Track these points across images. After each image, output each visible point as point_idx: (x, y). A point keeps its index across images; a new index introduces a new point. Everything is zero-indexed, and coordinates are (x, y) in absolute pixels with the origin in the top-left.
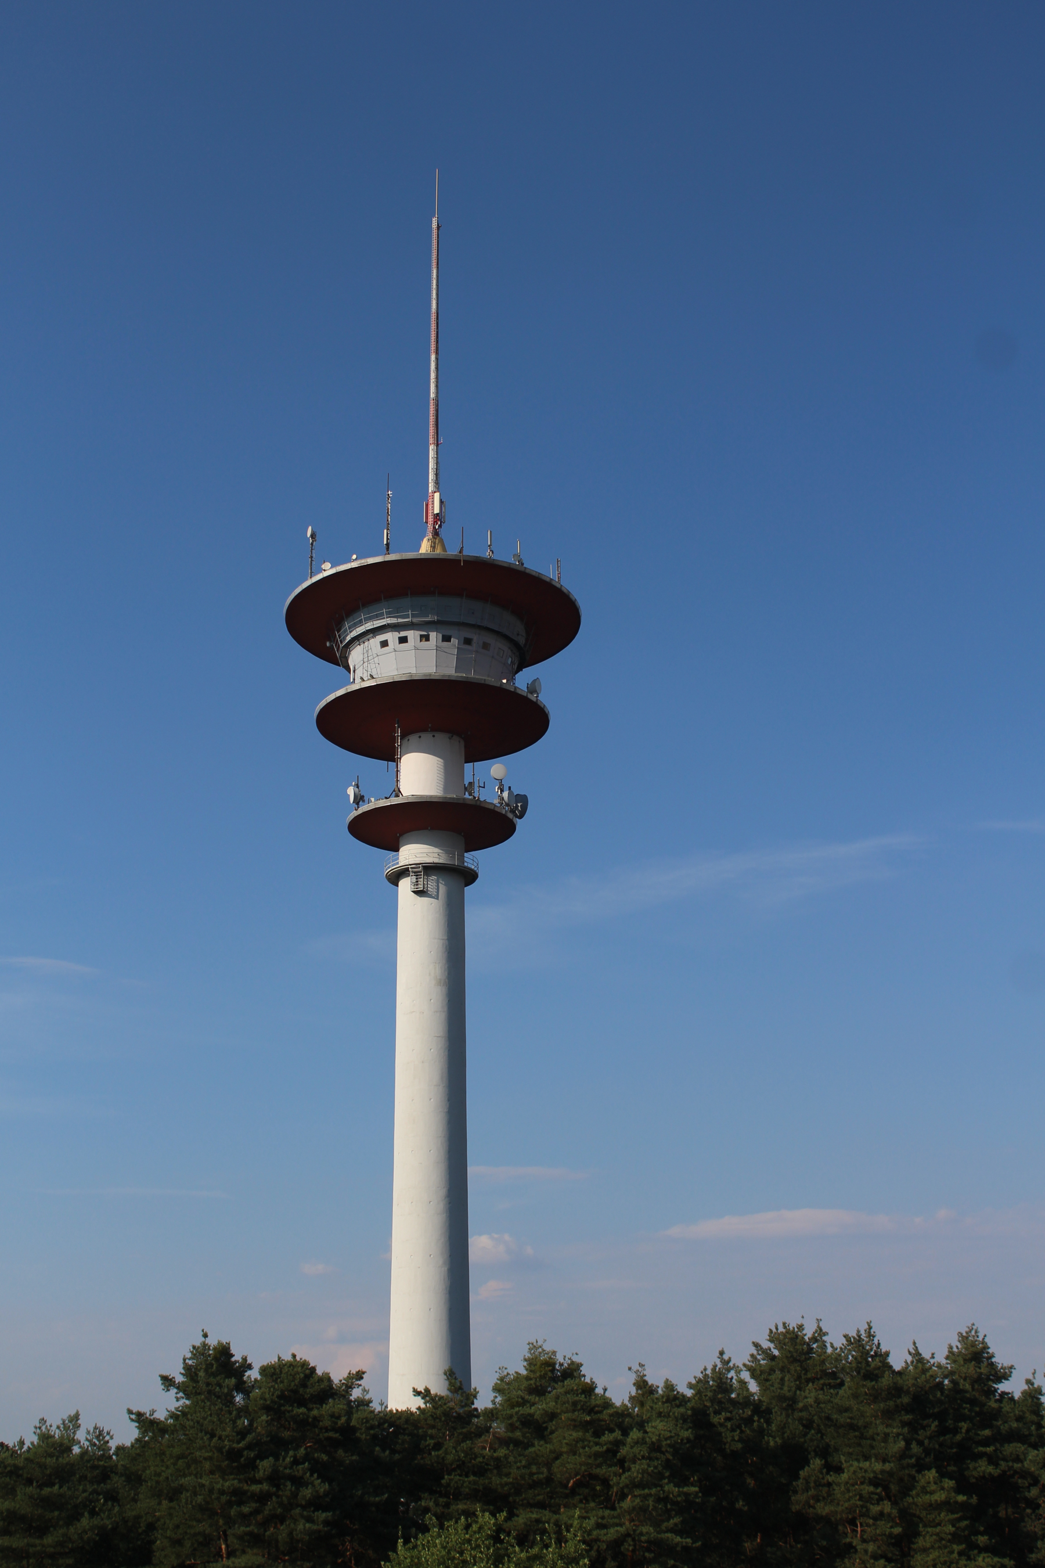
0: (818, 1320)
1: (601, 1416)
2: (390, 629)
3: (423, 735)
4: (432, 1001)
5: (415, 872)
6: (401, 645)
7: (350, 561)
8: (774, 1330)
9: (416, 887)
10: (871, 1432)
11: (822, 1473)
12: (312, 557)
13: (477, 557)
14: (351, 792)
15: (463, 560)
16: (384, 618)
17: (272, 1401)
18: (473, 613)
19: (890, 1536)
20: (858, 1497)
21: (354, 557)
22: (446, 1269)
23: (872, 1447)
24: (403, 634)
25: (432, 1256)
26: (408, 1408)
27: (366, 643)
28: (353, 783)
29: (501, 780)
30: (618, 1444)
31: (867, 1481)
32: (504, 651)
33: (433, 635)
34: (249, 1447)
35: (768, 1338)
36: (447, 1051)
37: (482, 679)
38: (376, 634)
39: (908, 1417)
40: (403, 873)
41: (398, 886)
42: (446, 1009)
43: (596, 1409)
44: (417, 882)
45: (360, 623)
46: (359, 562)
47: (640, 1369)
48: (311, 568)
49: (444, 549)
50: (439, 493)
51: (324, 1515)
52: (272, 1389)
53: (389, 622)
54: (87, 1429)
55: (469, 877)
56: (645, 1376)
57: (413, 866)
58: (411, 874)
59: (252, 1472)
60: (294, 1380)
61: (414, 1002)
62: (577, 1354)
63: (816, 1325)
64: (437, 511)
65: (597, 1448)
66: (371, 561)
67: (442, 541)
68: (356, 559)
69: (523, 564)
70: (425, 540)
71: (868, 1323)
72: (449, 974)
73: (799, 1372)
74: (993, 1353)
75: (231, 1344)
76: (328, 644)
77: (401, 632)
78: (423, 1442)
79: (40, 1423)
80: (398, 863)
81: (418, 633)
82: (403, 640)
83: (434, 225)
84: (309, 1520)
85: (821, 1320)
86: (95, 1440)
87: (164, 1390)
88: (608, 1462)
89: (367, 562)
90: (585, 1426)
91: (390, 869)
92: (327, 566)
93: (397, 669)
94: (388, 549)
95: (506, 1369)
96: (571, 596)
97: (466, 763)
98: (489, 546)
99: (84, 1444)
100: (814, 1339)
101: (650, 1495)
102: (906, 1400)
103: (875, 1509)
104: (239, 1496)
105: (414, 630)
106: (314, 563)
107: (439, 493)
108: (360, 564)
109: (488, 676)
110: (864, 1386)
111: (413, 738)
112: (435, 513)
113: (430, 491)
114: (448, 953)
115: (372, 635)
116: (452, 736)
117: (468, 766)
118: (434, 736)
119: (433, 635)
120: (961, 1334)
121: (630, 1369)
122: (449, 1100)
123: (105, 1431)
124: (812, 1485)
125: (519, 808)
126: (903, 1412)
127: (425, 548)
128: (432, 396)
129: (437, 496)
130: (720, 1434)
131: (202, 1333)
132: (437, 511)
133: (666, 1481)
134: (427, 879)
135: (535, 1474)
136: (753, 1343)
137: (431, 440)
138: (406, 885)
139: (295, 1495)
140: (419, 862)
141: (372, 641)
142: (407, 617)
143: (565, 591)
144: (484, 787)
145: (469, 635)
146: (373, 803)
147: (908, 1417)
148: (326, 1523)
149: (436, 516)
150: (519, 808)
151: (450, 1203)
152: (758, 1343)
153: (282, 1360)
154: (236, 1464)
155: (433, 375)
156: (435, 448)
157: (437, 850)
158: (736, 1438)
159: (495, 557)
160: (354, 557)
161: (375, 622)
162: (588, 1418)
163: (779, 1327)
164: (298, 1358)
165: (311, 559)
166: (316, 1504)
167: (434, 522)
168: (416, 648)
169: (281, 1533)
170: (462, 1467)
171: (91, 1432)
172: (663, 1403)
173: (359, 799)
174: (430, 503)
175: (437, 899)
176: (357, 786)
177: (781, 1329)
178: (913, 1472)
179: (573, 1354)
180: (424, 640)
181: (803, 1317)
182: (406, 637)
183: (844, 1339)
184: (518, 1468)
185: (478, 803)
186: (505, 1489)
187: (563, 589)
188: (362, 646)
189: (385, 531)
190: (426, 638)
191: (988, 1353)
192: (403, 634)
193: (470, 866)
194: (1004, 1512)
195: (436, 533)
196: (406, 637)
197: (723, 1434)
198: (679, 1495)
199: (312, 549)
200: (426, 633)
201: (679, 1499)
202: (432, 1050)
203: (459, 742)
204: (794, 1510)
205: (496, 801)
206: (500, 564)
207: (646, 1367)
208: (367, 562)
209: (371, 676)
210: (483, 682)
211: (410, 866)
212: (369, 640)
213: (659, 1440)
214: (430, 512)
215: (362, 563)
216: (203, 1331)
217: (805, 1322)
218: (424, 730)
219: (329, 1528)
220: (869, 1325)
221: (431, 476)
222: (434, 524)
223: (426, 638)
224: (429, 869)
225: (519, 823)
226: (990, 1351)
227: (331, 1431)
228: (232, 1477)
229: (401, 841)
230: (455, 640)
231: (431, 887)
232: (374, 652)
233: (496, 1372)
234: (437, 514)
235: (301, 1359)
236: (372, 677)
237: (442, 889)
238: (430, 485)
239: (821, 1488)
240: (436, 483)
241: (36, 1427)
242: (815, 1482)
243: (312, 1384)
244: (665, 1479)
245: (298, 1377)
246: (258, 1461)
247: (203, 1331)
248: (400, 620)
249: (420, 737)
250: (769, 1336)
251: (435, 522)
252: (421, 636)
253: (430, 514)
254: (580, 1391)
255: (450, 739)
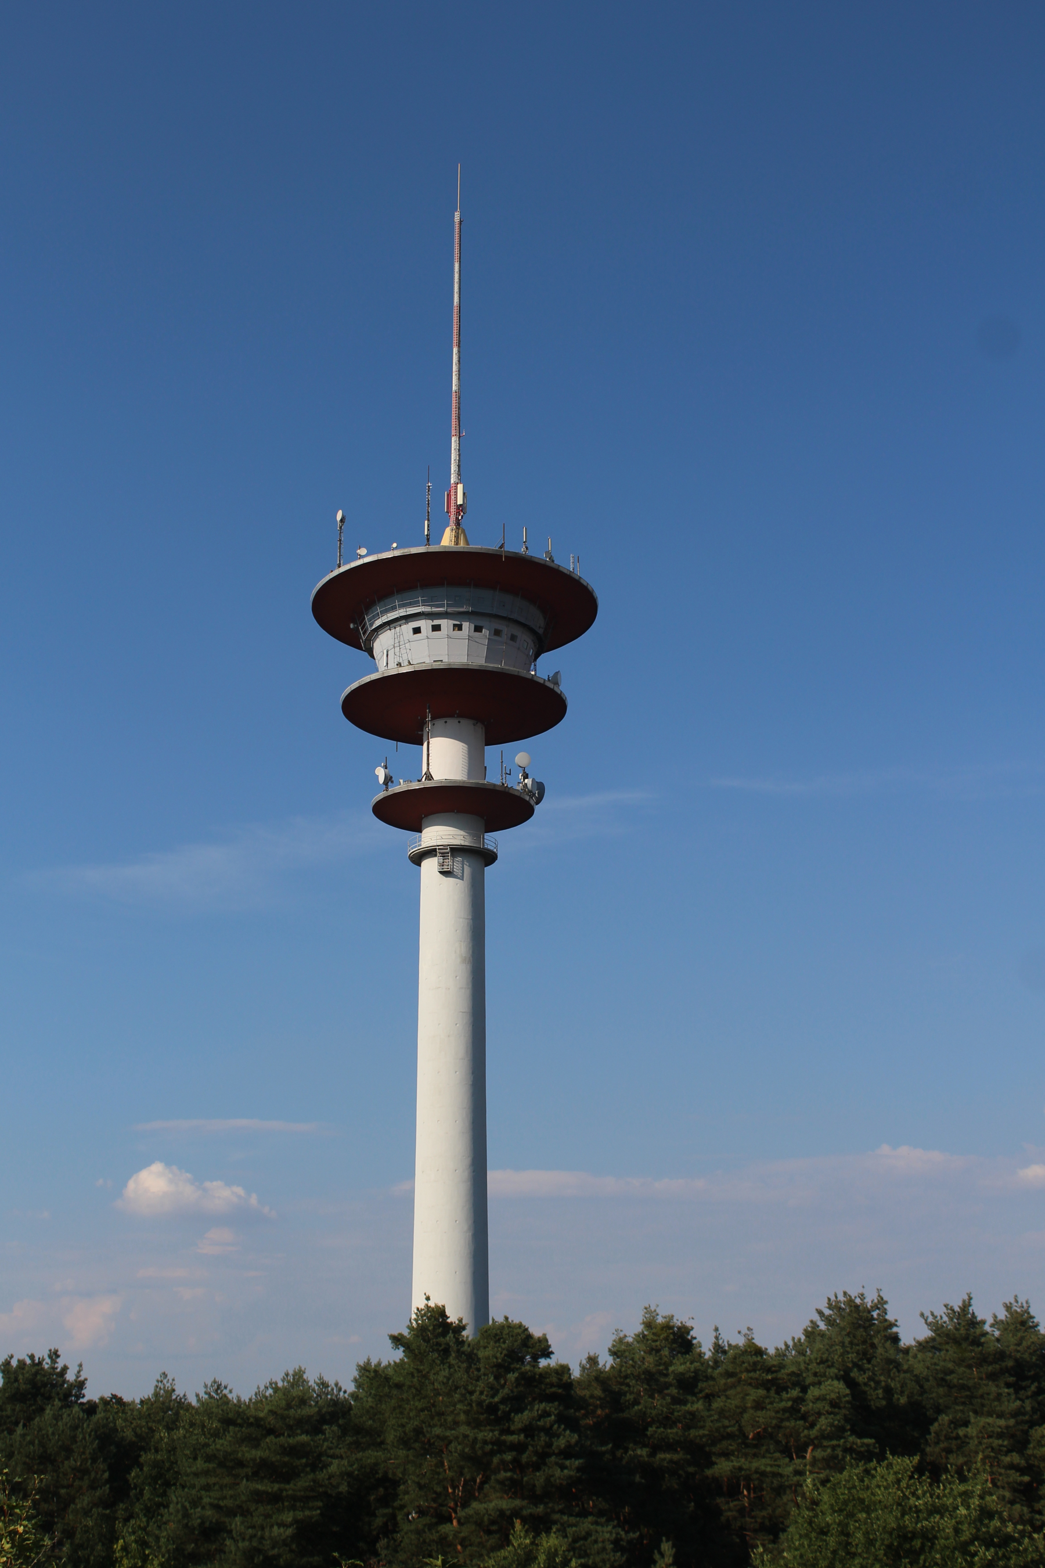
0: (878, 1290)
1: (779, 1375)
2: (424, 617)
3: (449, 720)
4: (458, 978)
5: (442, 853)
6: (434, 632)
7: (389, 549)
8: (833, 1298)
9: (441, 867)
10: (980, 1392)
11: (950, 1428)
12: (340, 540)
13: (516, 553)
14: (381, 773)
15: (505, 556)
16: (419, 606)
17: (503, 1360)
18: (504, 606)
19: (1021, 1483)
20: (990, 1450)
21: (395, 545)
22: (470, 1234)
23: (983, 1405)
24: (436, 622)
25: (457, 1222)
26: (300, 1367)
27: (398, 629)
28: (382, 764)
29: (524, 768)
30: (799, 1400)
31: (995, 1435)
32: (528, 643)
33: (466, 625)
34: (503, 1401)
35: (827, 1305)
36: (471, 1026)
37: (515, 671)
38: (409, 620)
39: (1012, 1379)
40: (430, 852)
41: (420, 866)
42: (470, 986)
43: (773, 1369)
44: (443, 862)
45: (394, 609)
46: (402, 552)
47: (748, 1333)
48: (340, 551)
49: (467, 542)
50: (462, 485)
51: (577, 1462)
52: (500, 1349)
53: (423, 610)
54: (205, 1383)
55: (489, 858)
56: (753, 1339)
57: (441, 847)
58: (438, 855)
59: (507, 1424)
60: (516, 1341)
61: (440, 978)
62: (693, 1318)
63: (877, 1294)
64: (460, 502)
65: (783, 1404)
66: (414, 550)
67: (464, 531)
68: (396, 548)
69: (553, 561)
70: (448, 531)
71: (967, 1294)
72: (473, 952)
73: (865, 1337)
74: (1038, 1322)
75: (446, 1307)
76: (352, 626)
77: (434, 621)
78: (623, 1397)
79: (161, 1376)
80: (420, 845)
81: (452, 622)
82: (436, 628)
83: (457, 219)
84: (563, 1467)
85: (881, 1290)
86: (213, 1394)
87: (393, 1348)
88: (794, 1416)
89: (410, 552)
90: (766, 1385)
91: (417, 849)
92: (363, 551)
93: (429, 656)
94: (428, 540)
95: (621, 1331)
96: (594, 594)
97: (486, 745)
98: (524, 542)
99: (202, 1397)
100: (876, 1307)
101: (839, 1446)
102: (1010, 1363)
103: (1007, 1459)
104: (500, 1446)
105: (447, 619)
106: (342, 546)
107: (462, 485)
108: (403, 553)
109: (514, 667)
110: (971, 1351)
111: (440, 723)
112: (458, 504)
113: (452, 482)
114: (473, 932)
115: (404, 621)
116: (477, 723)
117: (490, 750)
118: (459, 722)
119: (466, 625)
120: (1006, 1304)
121: (739, 1332)
122: (473, 1073)
123: (223, 1385)
124: (942, 1438)
125: (537, 795)
126: (1007, 1374)
127: (447, 540)
128: (454, 388)
129: (460, 487)
130: (865, 1392)
131: (425, 1296)
132: (460, 502)
133: (849, 1433)
134: (453, 860)
135: (727, 1427)
136: (817, 1310)
137: (453, 433)
138: (430, 867)
139: (549, 1445)
140: (447, 844)
141: (404, 627)
142: (442, 606)
143: (590, 589)
144: (510, 774)
145: (499, 627)
146: (401, 786)
147: (1012, 1379)
148: (578, 1469)
149: (460, 508)
150: (537, 795)
151: (474, 1172)
152: (820, 1310)
153: (496, 1322)
154: (493, 1417)
155: (455, 368)
156: (458, 439)
157: (462, 833)
158: (881, 1396)
159: (529, 553)
160: (395, 545)
161: (408, 610)
162: (770, 1377)
163: (838, 1296)
164: (510, 1320)
165: (340, 542)
166: (567, 1453)
167: (457, 513)
168: (449, 637)
169: (539, 1479)
170: (667, 1421)
171: (209, 1386)
172: (818, 1364)
173: (388, 780)
174: (452, 493)
175: (463, 880)
176: (386, 767)
177: (841, 1298)
178: (1026, 1427)
179: (689, 1318)
180: (457, 629)
181: (863, 1287)
182: (439, 626)
183: (945, 1308)
184: (712, 1421)
185: (507, 789)
186: (704, 1440)
187: (589, 587)
188: (393, 631)
189: (426, 522)
190: (459, 627)
191: (1033, 1322)
192: (436, 622)
193: (489, 847)
194: (75, 1484)
195: (458, 523)
196: (439, 626)
197: (868, 1392)
198: (862, 1446)
199: (340, 533)
200: (459, 623)
201: (862, 1449)
202: (458, 1025)
203: (482, 728)
204: (928, 1460)
205: (519, 787)
206: (537, 561)
207: (754, 1331)
208: (410, 552)
209: (409, 662)
210: (516, 674)
211: (437, 847)
212: (400, 626)
213: (839, 1398)
214: (453, 502)
215: (405, 552)
216: (425, 1294)
217: (865, 1291)
218: (451, 715)
219: (580, 1474)
220: (969, 1296)
221: (454, 468)
222: (457, 515)
223: (459, 627)
224: (456, 851)
225: (537, 808)
226: (1035, 1320)
227: (555, 1386)
228: (488, 1428)
229: (424, 822)
230: (486, 630)
231: (457, 868)
232: (406, 638)
233: (613, 1334)
234: (460, 505)
235: (512, 1321)
236: (410, 663)
237: (467, 870)
238: (452, 476)
239: (950, 1441)
240: (458, 474)
241: (158, 1381)
242: (945, 1436)
243: (532, 1344)
244: (847, 1432)
245: (520, 1337)
246: (513, 1414)
247: (425, 1294)
248: (435, 609)
249: (446, 722)
250: (828, 1304)
251: (458, 513)
252: (455, 625)
253: (452, 504)
254: (753, 1352)
255: (474, 725)
